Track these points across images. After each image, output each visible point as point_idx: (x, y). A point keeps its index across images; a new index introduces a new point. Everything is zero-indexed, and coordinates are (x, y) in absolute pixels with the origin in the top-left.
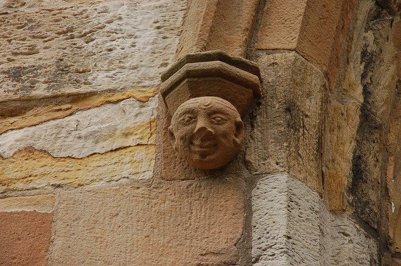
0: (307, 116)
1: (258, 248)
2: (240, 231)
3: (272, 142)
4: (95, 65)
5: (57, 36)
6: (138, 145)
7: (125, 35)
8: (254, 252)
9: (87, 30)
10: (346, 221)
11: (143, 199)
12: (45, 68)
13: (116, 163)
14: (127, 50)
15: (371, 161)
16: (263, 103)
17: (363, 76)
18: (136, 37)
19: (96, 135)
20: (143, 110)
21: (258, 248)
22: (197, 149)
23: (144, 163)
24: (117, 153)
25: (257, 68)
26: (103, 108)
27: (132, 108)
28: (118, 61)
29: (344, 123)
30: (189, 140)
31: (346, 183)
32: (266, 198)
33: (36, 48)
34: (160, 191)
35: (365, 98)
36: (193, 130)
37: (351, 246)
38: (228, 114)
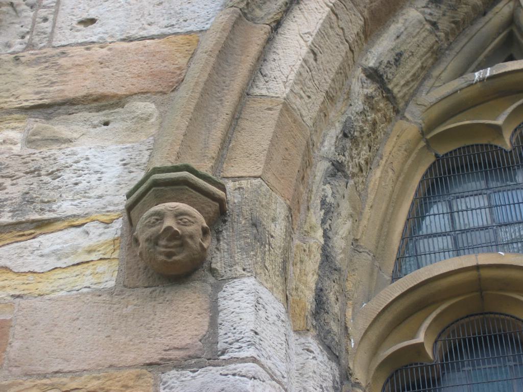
0: (272, 236)
1: (224, 342)
2: (206, 328)
3: (238, 252)
4: (61, 196)
5: (24, 175)
6: (101, 259)
7: (91, 171)
8: (221, 346)
9: (55, 169)
10: (310, 339)
11: (104, 305)
12: (11, 200)
13: (77, 275)
14: (93, 183)
15: (332, 297)
16: (229, 220)
17: (323, 222)
18: (102, 173)
19: (58, 253)
20: (106, 230)
21: (224, 342)
22: (163, 250)
23: (107, 275)
24: (79, 267)
25: (223, 185)
26: (66, 231)
27: (95, 229)
28: (83, 192)
29: (306, 258)
30: (154, 241)
31: (309, 307)
32: (233, 299)
33: (4, 185)
34: (123, 297)
35: (325, 241)
36: (159, 230)
37: (315, 362)
38: (195, 217)
